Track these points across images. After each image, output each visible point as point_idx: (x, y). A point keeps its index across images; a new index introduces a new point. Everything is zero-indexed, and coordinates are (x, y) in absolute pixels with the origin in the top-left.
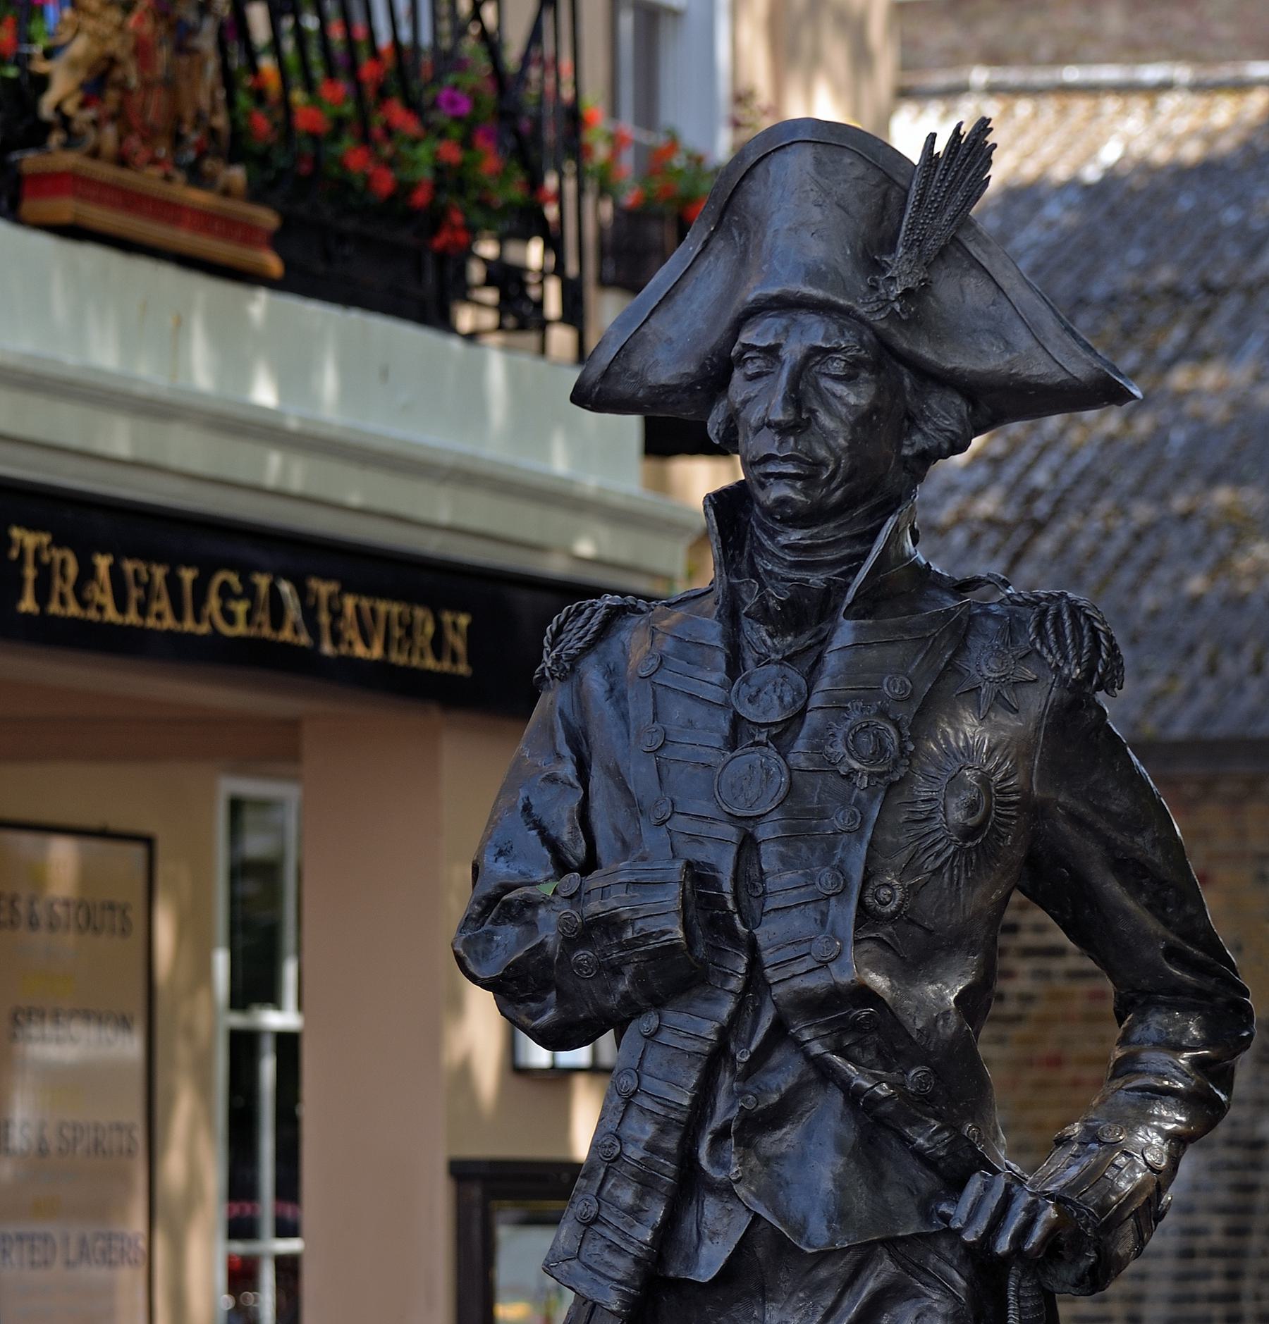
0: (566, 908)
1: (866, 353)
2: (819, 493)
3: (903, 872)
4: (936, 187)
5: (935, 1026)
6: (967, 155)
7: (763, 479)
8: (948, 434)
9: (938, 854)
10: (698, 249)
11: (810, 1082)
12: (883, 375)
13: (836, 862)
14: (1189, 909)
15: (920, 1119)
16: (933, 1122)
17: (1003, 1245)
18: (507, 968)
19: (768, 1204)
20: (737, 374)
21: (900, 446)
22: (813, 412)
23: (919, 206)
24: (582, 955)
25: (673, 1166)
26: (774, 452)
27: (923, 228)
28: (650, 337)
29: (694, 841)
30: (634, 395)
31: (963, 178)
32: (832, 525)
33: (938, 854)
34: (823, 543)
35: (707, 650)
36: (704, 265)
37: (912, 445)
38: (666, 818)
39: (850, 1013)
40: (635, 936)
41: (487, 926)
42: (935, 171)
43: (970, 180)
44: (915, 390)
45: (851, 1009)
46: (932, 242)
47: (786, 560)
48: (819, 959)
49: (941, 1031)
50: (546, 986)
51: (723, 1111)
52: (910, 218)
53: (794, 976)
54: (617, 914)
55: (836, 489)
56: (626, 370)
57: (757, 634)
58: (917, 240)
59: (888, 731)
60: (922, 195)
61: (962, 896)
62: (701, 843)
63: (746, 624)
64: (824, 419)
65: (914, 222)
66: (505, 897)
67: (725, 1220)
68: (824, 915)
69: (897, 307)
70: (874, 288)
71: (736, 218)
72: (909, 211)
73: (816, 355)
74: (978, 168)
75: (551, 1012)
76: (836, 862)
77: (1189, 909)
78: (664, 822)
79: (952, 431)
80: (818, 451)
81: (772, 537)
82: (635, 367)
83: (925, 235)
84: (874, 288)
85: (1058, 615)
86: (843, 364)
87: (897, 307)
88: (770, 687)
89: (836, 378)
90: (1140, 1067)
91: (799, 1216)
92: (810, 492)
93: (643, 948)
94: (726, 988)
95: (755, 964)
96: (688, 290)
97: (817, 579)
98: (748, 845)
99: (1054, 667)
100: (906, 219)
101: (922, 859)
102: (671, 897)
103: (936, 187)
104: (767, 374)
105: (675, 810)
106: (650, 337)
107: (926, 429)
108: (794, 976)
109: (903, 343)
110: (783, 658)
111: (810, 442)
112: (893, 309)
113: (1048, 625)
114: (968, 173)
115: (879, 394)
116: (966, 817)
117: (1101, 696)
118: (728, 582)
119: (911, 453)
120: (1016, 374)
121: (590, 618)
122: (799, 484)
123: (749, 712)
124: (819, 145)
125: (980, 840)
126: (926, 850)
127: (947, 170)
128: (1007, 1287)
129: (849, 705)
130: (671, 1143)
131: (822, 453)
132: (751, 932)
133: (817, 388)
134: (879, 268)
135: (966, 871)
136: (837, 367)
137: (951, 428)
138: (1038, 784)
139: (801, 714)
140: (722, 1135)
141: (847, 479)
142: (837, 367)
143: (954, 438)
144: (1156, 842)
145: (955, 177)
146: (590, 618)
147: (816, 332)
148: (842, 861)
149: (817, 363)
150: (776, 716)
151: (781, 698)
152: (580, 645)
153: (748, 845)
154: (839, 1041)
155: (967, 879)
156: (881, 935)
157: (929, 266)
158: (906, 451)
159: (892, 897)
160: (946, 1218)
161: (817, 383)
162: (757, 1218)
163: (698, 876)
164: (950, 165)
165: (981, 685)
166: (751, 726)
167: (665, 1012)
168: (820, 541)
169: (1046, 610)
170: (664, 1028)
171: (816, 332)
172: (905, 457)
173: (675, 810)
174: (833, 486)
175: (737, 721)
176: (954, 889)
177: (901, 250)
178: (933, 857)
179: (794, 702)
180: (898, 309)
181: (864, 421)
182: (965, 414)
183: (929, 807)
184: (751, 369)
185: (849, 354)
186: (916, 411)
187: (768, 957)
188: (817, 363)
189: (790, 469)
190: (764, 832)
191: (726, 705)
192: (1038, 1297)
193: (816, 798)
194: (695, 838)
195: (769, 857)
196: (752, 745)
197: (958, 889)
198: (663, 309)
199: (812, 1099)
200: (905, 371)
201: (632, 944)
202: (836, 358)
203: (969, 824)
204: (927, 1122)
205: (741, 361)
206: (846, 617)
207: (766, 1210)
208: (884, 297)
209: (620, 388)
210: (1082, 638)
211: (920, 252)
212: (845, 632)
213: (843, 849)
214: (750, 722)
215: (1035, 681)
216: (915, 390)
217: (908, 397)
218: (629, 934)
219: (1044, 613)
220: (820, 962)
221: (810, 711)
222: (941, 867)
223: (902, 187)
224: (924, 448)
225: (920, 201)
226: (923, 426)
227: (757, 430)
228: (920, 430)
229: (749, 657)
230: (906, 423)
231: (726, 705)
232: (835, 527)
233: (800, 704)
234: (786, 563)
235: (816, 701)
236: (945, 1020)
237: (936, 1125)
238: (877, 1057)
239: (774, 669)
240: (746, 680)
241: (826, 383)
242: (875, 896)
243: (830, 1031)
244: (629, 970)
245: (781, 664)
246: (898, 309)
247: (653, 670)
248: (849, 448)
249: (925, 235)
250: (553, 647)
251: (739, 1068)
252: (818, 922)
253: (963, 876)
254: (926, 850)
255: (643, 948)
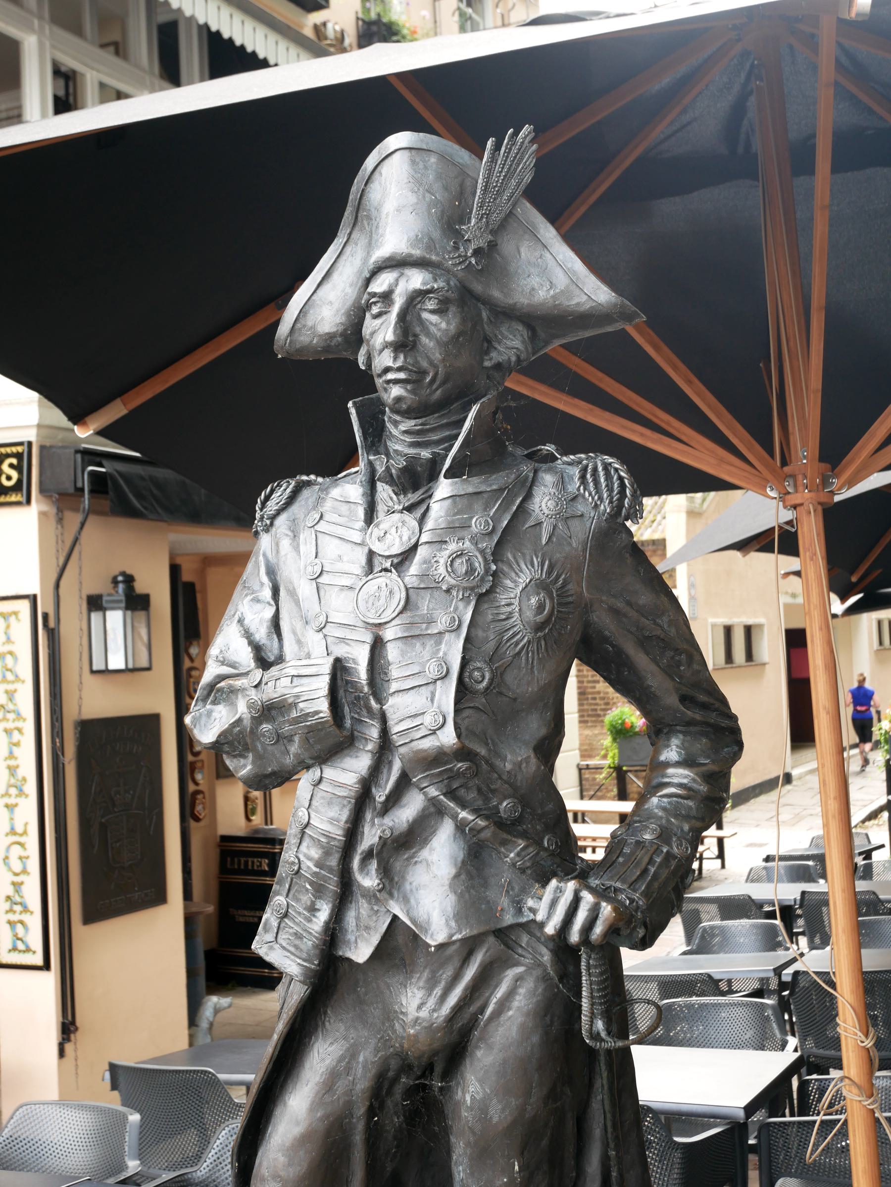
0: (253, 694)
1: (453, 292)
2: (425, 392)
3: (491, 661)
4: (497, 177)
5: (520, 768)
6: (517, 153)
7: (385, 385)
8: (515, 350)
9: (517, 643)
10: (345, 239)
11: (430, 814)
12: (466, 309)
13: (441, 654)
14: (696, 667)
15: (511, 840)
16: (520, 841)
17: (574, 937)
18: (219, 736)
19: (402, 907)
20: (368, 315)
21: (482, 361)
22: (416, 336)
23: (485, 190)
24: (266, 727)
25: (335, 879)
26: (390, 363)
27: (489, 206)
28: (318, 302)
29: (341, 642)
30: (311, 341)
31: (515, 170)
32: (436, 415)
33: (517, 643)
34: (430, 428)
35: (352, 505)
36: (348, 249)
37: (491, 359)
38: (322, 626)
39: (455, 765)
40: (298, 715)
41: (208, 707)
42: (495, 166)
43: (520, 172)
44: (491, 321)
45: (456, 763)
46: (495, 215)
47: (405, 441)
48: (430, 727)
49: (524, 770)
50: (247, 749)
51: (370, 836)
52: (480, 198)
53: (412, 741)
54: (285, 699)
55: (437, 389)
56: (304, 326)
57: (384, 491)
58: (485, 214)
59: (476, 557)
60: (487, 182)
61: (536, 672)
62: (347, 644)
63: (380, 486)
64: (424, 340)
65: (482, 201)
66: (219, 685)
67: (374, 918)
68: (433, 695)
69: (473, 261)
70: (456, 248)
71: (365, 213)
72: (478, 194)
73: (418, 296)
74: (526, 162)
75: (249, 767)
76: (441, 654)
77: (696, 667)
78: (321, 630)
79: (517, 348)
80: (421, 362)
81: (396, 427)
82: (310, 323)
83: (490, 210)
84: (456, 248)
85: (595, 470)
86: (436, 301)
87: (473, 261)
88: (394, 529)
89: (433, 312)
90: (666, 780)
91: (425, 917)
92: (418, 392)
93: (303, 724)
94: (366, 749)
95: (385, 733)
96: (340, 269)
97: (426, 454)
98: (377, 646)
99: (671, 838)
100: (476, 200)
101: (505, 648)
102: (323, 684)
103: (497, 177)
104: (386, 313)
105: (329, 620)
106: (318, 302)
107: (499, 347)
108: (412, 741)
109: (478, 287)
110: (404, 509)
111: (416, 357)
112: (470, 262)
113: (588, 476)
114: (518, 166)
115: (464, 320)
116: (535, 616)
117: (628, 523)
118: (368, 460)
119: (490, 365)
120: (559, 305)
121: (285, 490)
122: (409, 387)
123: (377, 548)
124: (413, 151)
125: (547, 631)
126: (508, 640)
127: (504, 165)
128: (582, 984)
129: (447, 539)
130: (334, 861)
131: (425, 364)
132: (381, 708)
133: (419, 318)
134: (458, 234)
135: (538, 654)
136: (431, 305)
137: (516, 346)
138: (587, 590)
139: (415, 547)
140: (368, 855)
141: (444, 383)
142: (431, 305)
143: (518, 353)
144: (670, 623)
145: (509, 169)
146: (285, 490)
147: (416, 279)
148: (445, 654)
149: (419, 302)
150: (396, 550)
151: (401, 537)
152: (277, 508)
153: (377, 646)
154: (448, 786)
155: (539, 659)
156: (477, 705)
157: (494, 232)
158: (487, 364)
159: (483, 677)
160: (533, 911)
161: (420, 316)
162: (395, 918)
163: (340, 669)
164: (506, 161)
165: (543, 520)
166: (380, 558)
167: (323, 766)
168: (428, 427)
169: (587, 466)
170: (324, 780)
171: (416, 279)
172: (486, 368)
173: (329, 620)
174: (434, 387)
175: (371, 554)
176: (530, 666)
177: (473, 221)
178: (513, 646)
179: (410, 539)
180: (474, 262)
181: (453, 343)
182: (526, 337)
183: (509, 609)
184: (375, 310)
185: (440, 294)
186: (491, 335)
187: (395, 729)
188: (419, 302)
189: (402, 375)
190: (389, 634)
191: (362, 544)
192: (604, 964)
193: (426, 607)
194: (343, 640)
195: (392, 652)
196: (381, 572)
197: (533, 667)
198: (325, 282)
199: (433, 826)
200: (482, 306)
201: (297, 721)
202: (432, 298)
203: (538, 621)
204: (515, 842)
205: (368, 306)
206: (445, 477)
207: (401, 912)
208: (463, 254)
209: (302, 338)
210: (613, 484)
211: (488, 222)
212: (444, 488)
213: (446, 645)
214: (380, 555)
215: (368, 282)
216: (491, 321)
217: (485, 326)
218: (294, 714)
219: (584, 470)
220: (430, 730)
221: (421, 545)
222: (519, 653)
223: (473, 178)
224: (499, 362)
225: (486, 186)
226: (497, 346)
227: (381, 351)
228: (495, 348)
229: (381, 508)
230: (486, 345)
231: (362, 544)
232: (439, 417)
233: (413, 541)
234: (406, 444)
235: (424, 538)
236: (527, 763)
237: (522, 844)
238: (478, 794)
239: (396, 516)
240: (377, 525)
241: (425, 315)
242: (471, 677)
243: (441, 779)
244: (297, 739)
245: (402, 513)
246: (474, 262)
247: (316, 521)
248: (443, 360)
249: (490, 210)
250: (261, 510)
251: (379, 806)
252: (429, 699)
253: (536, 658)
254: (508, 640)
255: (303, 724)
